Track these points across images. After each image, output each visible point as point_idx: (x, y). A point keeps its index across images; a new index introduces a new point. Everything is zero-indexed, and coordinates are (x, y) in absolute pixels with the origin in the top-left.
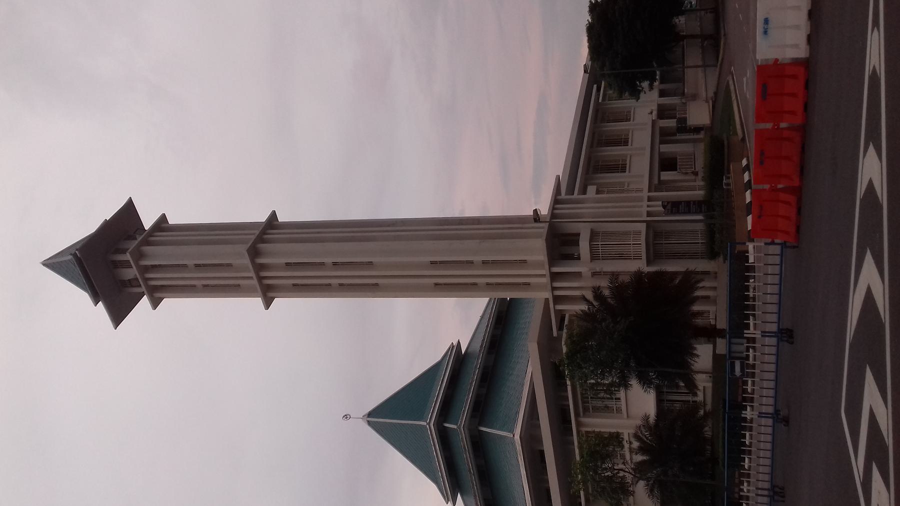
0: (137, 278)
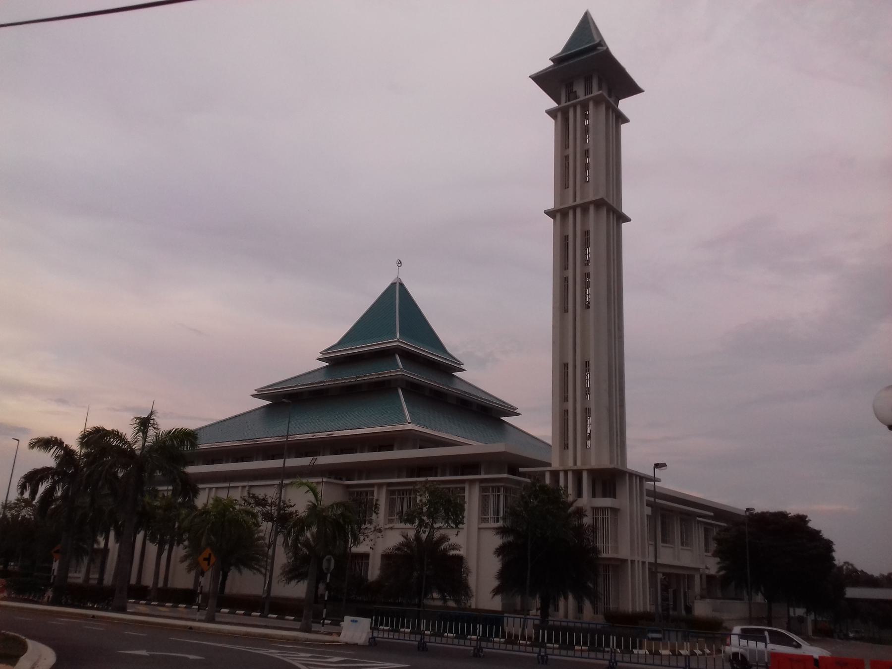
0: (577, 99)
